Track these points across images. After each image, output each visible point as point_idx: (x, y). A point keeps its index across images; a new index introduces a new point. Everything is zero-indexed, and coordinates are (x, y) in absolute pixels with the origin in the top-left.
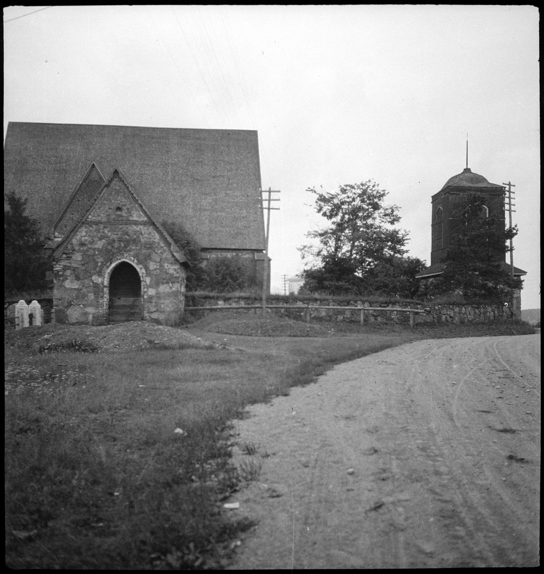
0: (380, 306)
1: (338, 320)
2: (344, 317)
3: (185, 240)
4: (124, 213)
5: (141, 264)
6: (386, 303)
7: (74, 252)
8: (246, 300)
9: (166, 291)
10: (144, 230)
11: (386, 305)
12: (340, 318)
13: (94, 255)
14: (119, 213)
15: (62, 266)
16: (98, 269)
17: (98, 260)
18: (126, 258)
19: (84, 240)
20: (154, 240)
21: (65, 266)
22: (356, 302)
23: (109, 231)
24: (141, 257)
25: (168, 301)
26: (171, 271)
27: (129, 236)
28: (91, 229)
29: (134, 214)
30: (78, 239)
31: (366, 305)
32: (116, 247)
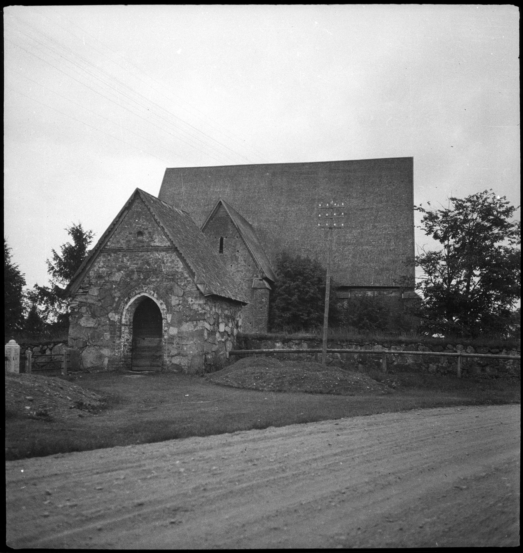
0: (489, 352)
1: (430, 370)
2: (438, 366)
3: (317, 278)
4: (145, 238)
5: (161, 298)
6: (498, 347)
7: (91, 286)
8: (309, 342)
9: (190, 329)
10: (166, 257)
11: (497, 350)
12: (433, 367)
13: (111, 289)
14: (140, 238)
15: (78, 303)
16: (115, 305)
17: (116, 295)
18: (145, 292)
19: (102, 271)
20: (177, 270)
21: (82, 302)
22: (454, 346)
23: (128, 260)
24: (162, 291)
25: (192, 342)
26: (195, 307)
27: (149, 265)
28: (109, 258)
29: (156, 238)
30: (96, 270)
31: (468, 350)
32: (135, 279)
